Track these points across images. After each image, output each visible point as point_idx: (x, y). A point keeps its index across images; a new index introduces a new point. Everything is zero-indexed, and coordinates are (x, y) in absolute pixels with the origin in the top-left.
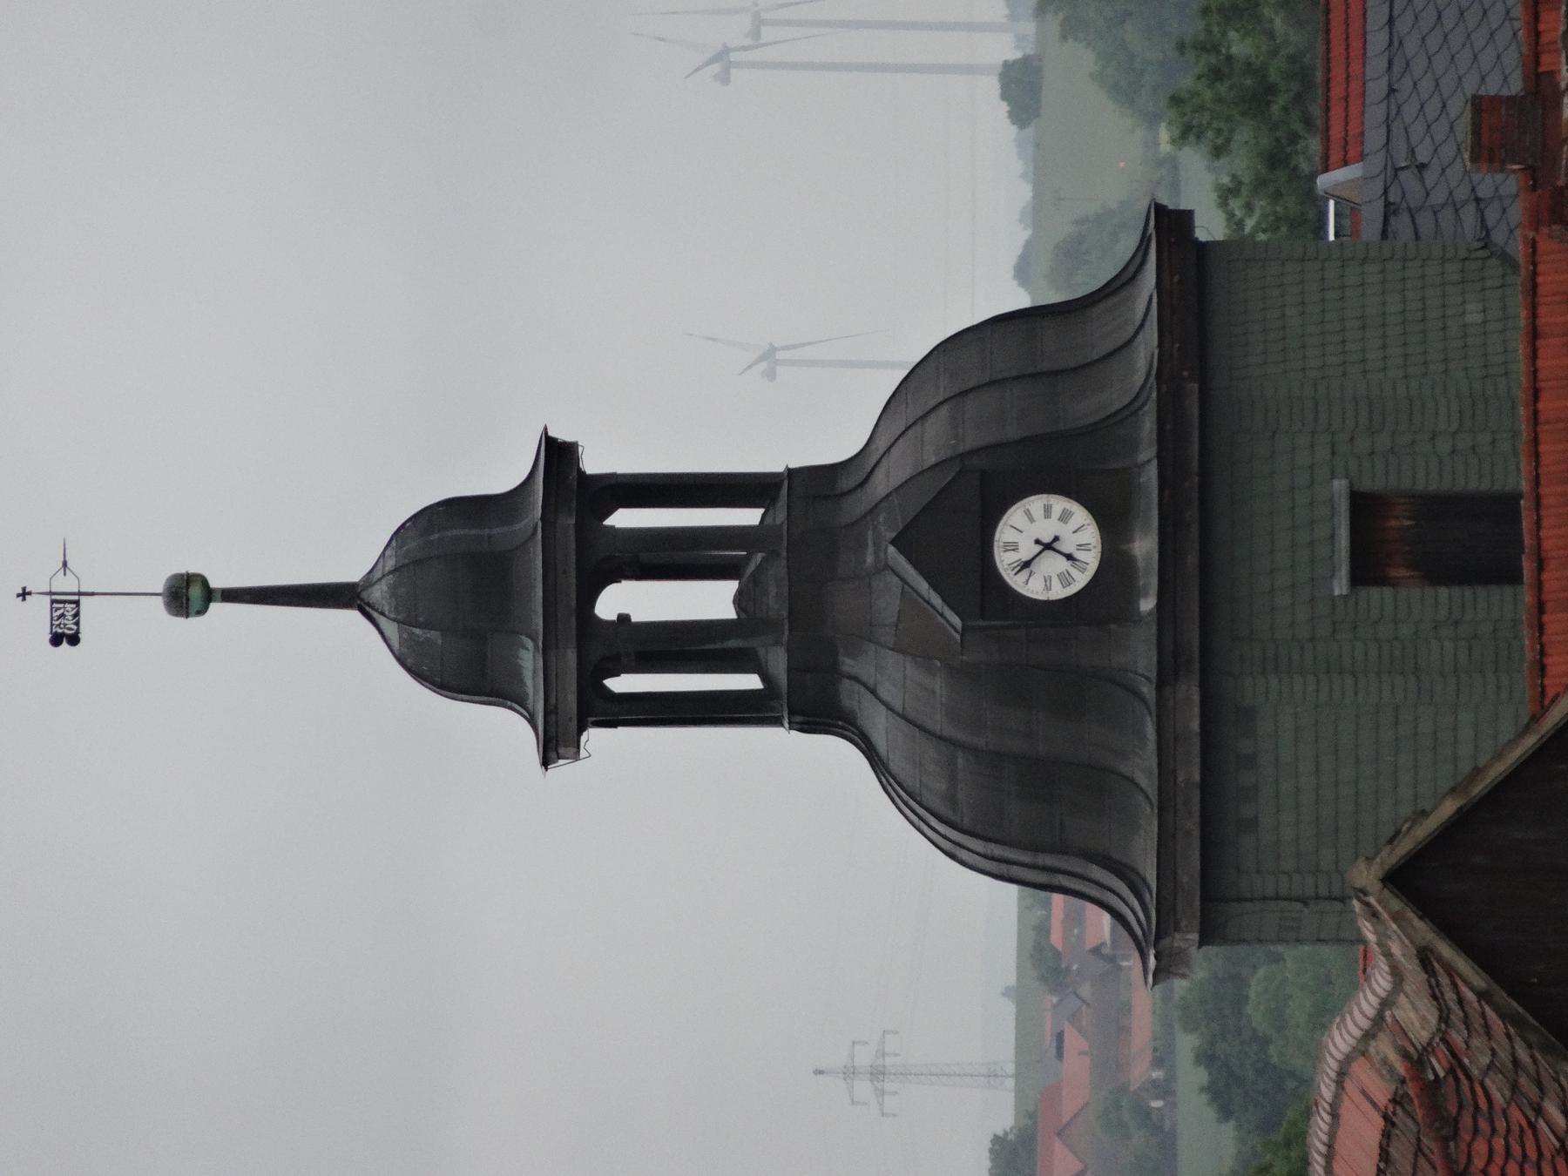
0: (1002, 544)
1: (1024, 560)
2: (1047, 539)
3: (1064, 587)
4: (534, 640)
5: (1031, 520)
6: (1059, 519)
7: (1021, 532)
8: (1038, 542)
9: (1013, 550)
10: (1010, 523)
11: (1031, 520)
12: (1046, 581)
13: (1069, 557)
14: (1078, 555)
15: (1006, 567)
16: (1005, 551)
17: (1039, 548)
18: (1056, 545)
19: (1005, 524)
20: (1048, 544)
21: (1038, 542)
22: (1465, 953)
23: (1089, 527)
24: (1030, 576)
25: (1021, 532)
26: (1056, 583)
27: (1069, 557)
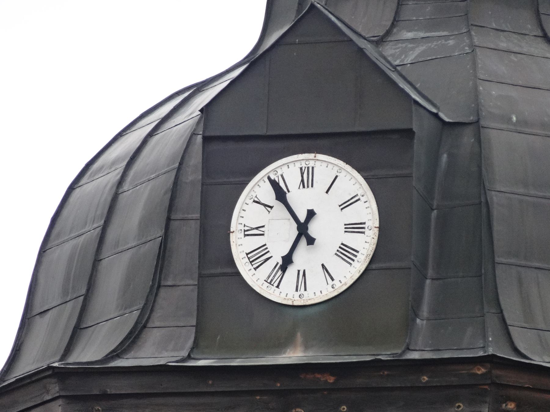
0: (311, 164)
1: (288, 196)
2: (313, 229)
3: (247, 254)
4: (189, 357)
5: (344, 206)
6: (356, 257)
7: (327, 192)
8: (311, 214)
9: (302, 181)
10: (341, 176)
11: (344, 206)
12: (257, 228)
13: (287, 260)
14: (291, 271)
15: (280, 173)
16: (301, 169)
17: (302, 217)
18: (303, 241)
19: (341, 168)
20: (298, 229)
21: (311, 214)
22: (274, 44)
23: (329, 287)
24: (265, 205)
25: (327, 192)
26: (254, 242)
27: (287, 260)
